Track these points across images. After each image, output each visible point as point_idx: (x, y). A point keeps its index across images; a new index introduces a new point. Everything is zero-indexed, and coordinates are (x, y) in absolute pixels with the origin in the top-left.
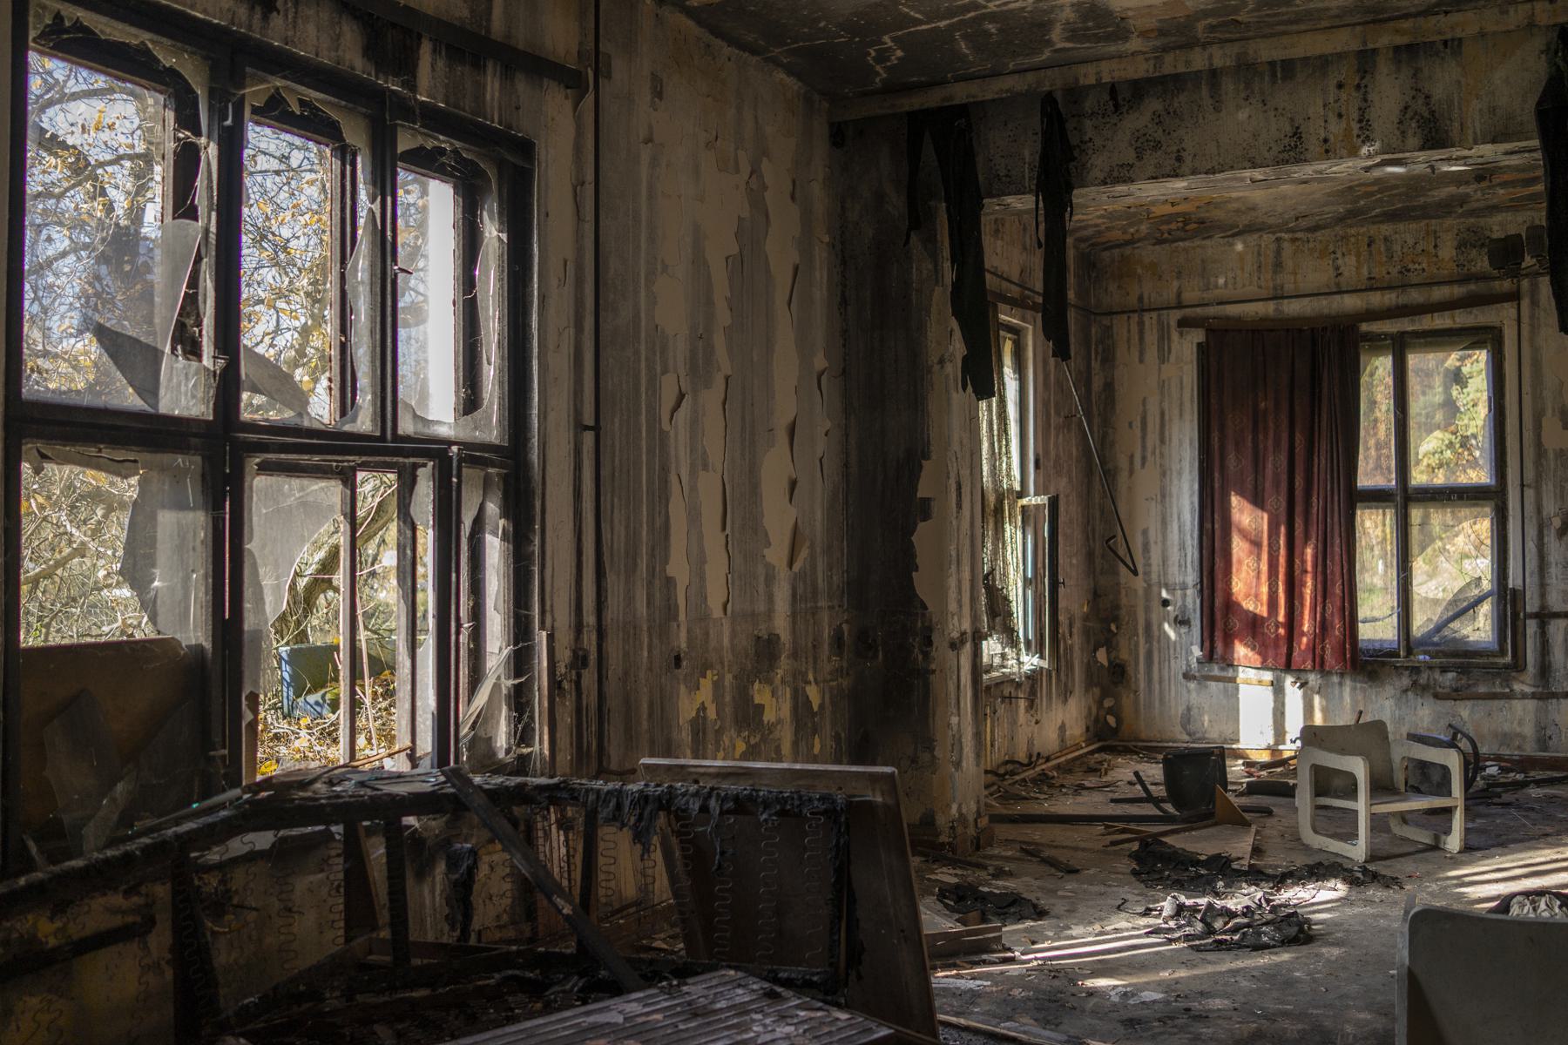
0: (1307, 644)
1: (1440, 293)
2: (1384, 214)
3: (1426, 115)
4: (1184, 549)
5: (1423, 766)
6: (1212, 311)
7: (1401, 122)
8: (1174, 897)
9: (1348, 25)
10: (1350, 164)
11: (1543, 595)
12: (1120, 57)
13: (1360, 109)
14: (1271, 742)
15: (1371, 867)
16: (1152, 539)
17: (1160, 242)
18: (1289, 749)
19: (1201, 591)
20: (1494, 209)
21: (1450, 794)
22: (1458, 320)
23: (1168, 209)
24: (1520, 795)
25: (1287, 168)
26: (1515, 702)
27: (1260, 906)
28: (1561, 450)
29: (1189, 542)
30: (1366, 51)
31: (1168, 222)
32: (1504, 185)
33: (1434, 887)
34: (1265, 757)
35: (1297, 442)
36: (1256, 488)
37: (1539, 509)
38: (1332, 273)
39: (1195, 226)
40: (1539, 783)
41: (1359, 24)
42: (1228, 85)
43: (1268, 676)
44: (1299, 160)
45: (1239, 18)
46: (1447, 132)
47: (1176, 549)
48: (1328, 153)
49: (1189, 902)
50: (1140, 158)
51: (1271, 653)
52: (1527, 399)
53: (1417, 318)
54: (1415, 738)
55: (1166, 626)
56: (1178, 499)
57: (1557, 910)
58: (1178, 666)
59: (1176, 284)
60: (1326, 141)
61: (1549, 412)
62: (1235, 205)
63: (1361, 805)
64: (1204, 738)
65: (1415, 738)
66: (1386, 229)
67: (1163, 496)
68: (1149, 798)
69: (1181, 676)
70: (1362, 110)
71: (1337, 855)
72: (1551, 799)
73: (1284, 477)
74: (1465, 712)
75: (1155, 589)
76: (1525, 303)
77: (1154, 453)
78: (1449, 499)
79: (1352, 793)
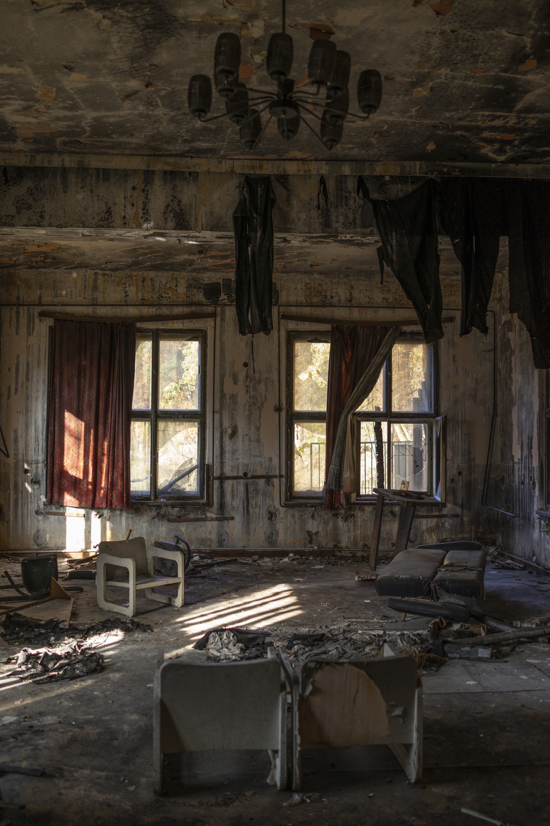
0: (104, 494)
1: (178, 310)
2: (151, 266)
3: (178, 211)
4: (38, 441)
5: (163, 561)
6: (58, 309)
7: (165, 213)
8: (25, 651)
9: (140, 155)
10: (137, 232)
11: (222, 468)
12: (10, 152)
13: (144, 203)
14: (83, 547)
15: (136, 620)
16: (19, 435)
17: (30, 267)
18: (93, 552)
19: (47, 465)
20: (206, 269)
21: (176, 576)
22: (185, 325)
23: (35, 249)
24: (210, 571)
25: (103, 230)
26: (207, 522)
27: (75, 650)
28: (233, 394)
29: (40, 437)
30: (149, 171)
31: (36, 257)
32: (212, 257)
33: (169, 629)
34: (80, 556)
35: (102, 384)
36: (78, 408)
37: (221, 424)
38: (123, 294)
39: (52, 260)
40: (219, 564)
41: (146, 155)
42: (72, 178)
43: (82, 512)
44: (109, 227)
45: (81, 140)
46: (188, 222)
47: (33, 441)
48: (125, 225)
49: (34, 652)
50: (19, 213)
51: (84, 499)
52: (217, 368)
53: (165, 322)
54: (159, 545)
55: (27, 484)
56: (35, 413)
57: (231, 638)
58: (32, 507)
59: (38, 292)
60: (124, 218)
61: (227, 375)
62: (74, 251)
63: (131, 585)
64: (47, 547)
65: (159, 545)
66: (152, 274)
67: (27, 411)
68: (13, 586)
69: (34, 513)
70: (145, 204)
71: (118, 613)
72: (225, 573)
73: (94, 403)
74: (183, 528)
75: (21, 463)
76: (218, 319)
77: (22, 386)
78: (178, 417)
79: (126, 578)
